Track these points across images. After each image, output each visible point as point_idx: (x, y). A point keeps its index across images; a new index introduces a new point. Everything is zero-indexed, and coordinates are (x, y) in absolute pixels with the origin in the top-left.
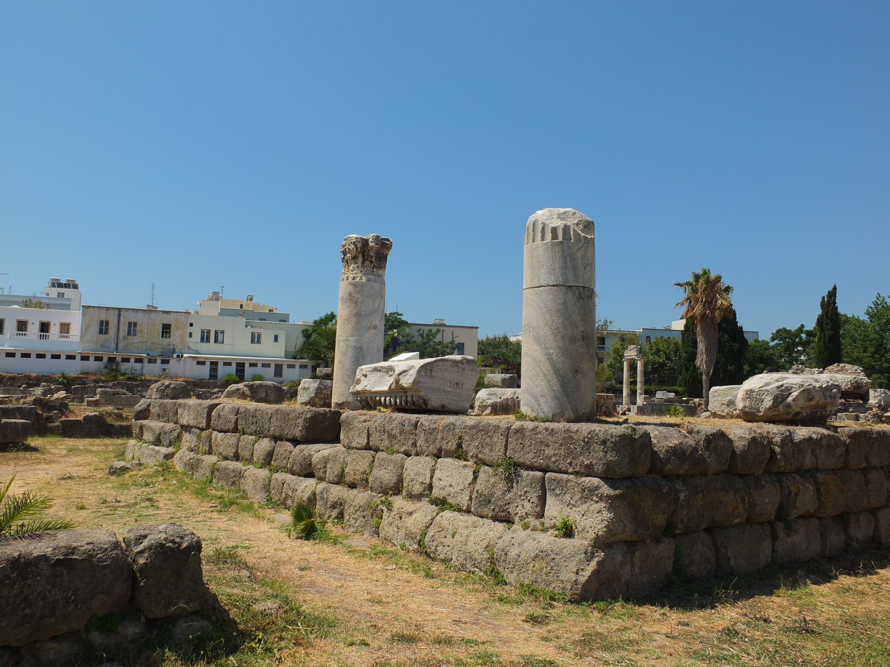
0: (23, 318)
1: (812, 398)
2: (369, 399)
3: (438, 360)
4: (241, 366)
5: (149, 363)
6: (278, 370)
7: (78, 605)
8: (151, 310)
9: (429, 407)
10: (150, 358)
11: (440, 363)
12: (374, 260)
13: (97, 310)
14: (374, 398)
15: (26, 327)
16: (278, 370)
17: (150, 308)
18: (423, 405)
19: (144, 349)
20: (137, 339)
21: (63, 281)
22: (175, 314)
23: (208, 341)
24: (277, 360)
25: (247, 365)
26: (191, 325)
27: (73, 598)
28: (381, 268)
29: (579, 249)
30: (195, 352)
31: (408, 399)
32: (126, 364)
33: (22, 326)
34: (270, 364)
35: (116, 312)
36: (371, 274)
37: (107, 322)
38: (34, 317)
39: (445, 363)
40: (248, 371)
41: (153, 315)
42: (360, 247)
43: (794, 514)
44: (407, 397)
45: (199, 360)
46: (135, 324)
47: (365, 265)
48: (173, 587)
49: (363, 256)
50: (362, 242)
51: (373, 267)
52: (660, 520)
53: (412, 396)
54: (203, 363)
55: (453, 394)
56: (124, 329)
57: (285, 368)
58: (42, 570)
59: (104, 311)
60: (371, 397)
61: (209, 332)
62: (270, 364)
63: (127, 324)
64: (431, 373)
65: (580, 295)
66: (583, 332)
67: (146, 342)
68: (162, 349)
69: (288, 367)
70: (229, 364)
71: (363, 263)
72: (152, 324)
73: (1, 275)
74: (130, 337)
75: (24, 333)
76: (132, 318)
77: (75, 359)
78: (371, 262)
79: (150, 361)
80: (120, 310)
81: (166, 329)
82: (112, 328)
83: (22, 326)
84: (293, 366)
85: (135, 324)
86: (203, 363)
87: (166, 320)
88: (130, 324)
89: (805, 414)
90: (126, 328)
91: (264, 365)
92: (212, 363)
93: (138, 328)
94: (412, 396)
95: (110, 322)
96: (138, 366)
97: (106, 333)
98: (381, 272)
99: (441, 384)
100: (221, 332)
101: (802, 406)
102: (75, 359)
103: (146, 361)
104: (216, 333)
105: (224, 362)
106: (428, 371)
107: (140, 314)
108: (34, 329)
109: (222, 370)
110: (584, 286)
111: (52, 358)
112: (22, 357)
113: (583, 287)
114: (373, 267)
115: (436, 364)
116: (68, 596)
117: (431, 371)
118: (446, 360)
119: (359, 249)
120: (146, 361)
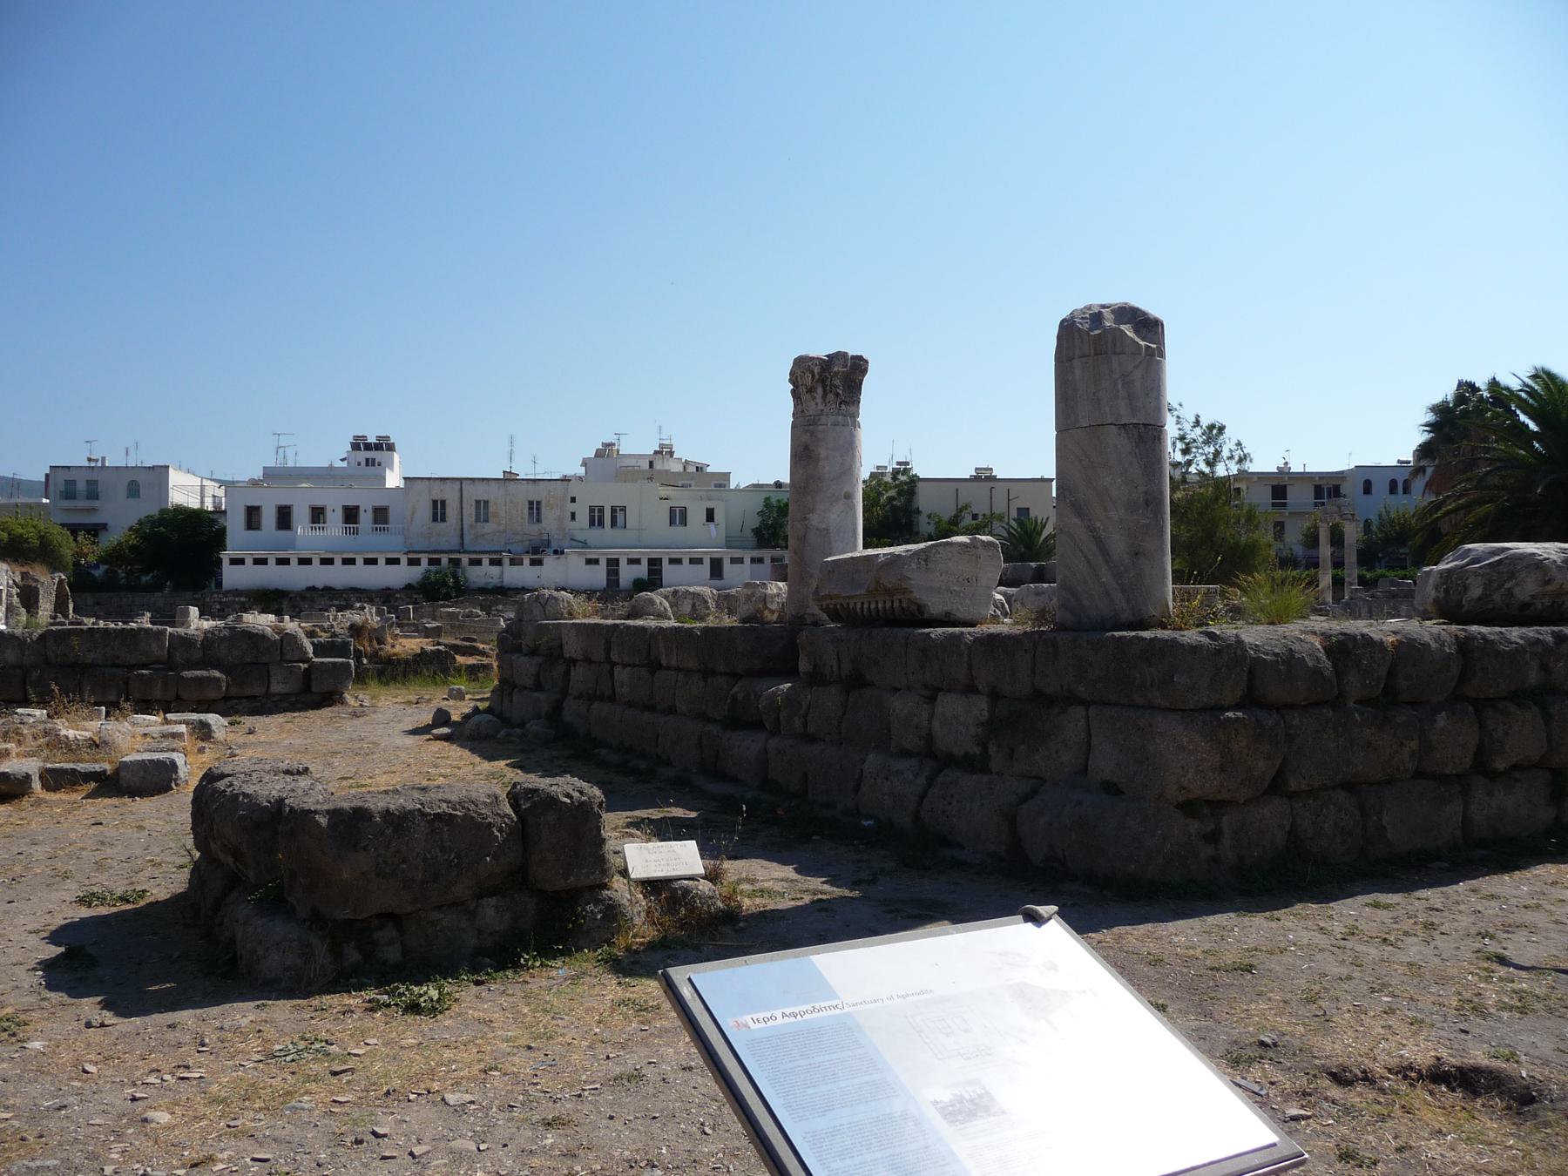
0: (319, 503)
1: (1549, 580)
2: (838, 607)
3: (937, 545)
4: (655, 563)
5: (511, 565)
6: (716, 568)
7: (462, 870)
8: (509, 478)
9: (926, 616)
10: (512, 556)
11: (940, 549)
12: (841, 392)
13: (427, 482)
14: (845, 606)
15: (279, 511)
16: (716, 568)
17: (507, 476)
18: (917, 613)
19: (503, 543)
20: (488, 528)
21: (372, 439)
22: (546, 482)
23: (601, 524)
24: (712, 552)
25: (665, 562)
26: (573, 500)
27: (456, 861)
28: (853, 403)
29: (1137, 367)
30: (581, 544)
31: (895, 605)
32: (476, 568)
33: (317, 514)
34: (702, 559)
35: (457, 486)
36: (838, 414)
37: (443, 503)
38: (334, 502)
39: (948, 548)
40: (668, 571)
41: (512, 486)
42: (818, 373)
43: (1500, 765)
44: (893, 602)
45: (589, 557)
46: (486, 502)
47: (827, 400)
48: (572, 853)
49: (824, 387)
50: (820, 364)
51: (841, 403)
52: (1263, 767)
53: (900, 600)
54: (596, 562)
55: (961, 595)
56: (470, 511)
57: (726, 564)
58: (419, 826)
59: (437, 485)
60: (842, 605)
61: (601, 509)
62: (702, 559)
63: (474, 503)
64: (927, 565)
65: (1140, 436)
66: (1146, 493)
67: (505, 531)
68: (530, 540)
69: (731, 563)
70: (636, 561)
71: (824, 397)
72: (511, 502)
73: (1563, 966)
74: (479, 524)
75: (321, 525)
76: (481, 493)
77: (399, 564)
78: (837, 395)
79: (513, 562)
80: (461, 480)
81: (535, 508)
82: (452, 512)
83: (317, 514)
84: (740, 561)
85: (486, 502)
86: (596, 562)
87: (535, 494)
88: (478, 502)
89: (1539, 606)
90: (473, 510)
91: (692, 561)
92: (712, 560)
93: (491, 509)
94: (900, 600)
95: (447, 502)
96: (495, 570)
97: (443, 520)
98: (852, 409)
99: (943, 581)
100: (620, 510)
101: (1533, 593)
102: (399, 564)
103: (506, 561)
104: (613, 510)
105: (387, 559)
106: (923, 562)
107: (493, 486)
108: (335, 518)
109: (627, 574)
110: (1145, 422)
111: (321, 564)
112: (365, 564)
113: (1143, 424)
114: (841, 403)
115: (934, 551)
116: (451, 858)
117: (926, 560)
118: (951, 544)
119: (817, 377)
120: (506, 561)
